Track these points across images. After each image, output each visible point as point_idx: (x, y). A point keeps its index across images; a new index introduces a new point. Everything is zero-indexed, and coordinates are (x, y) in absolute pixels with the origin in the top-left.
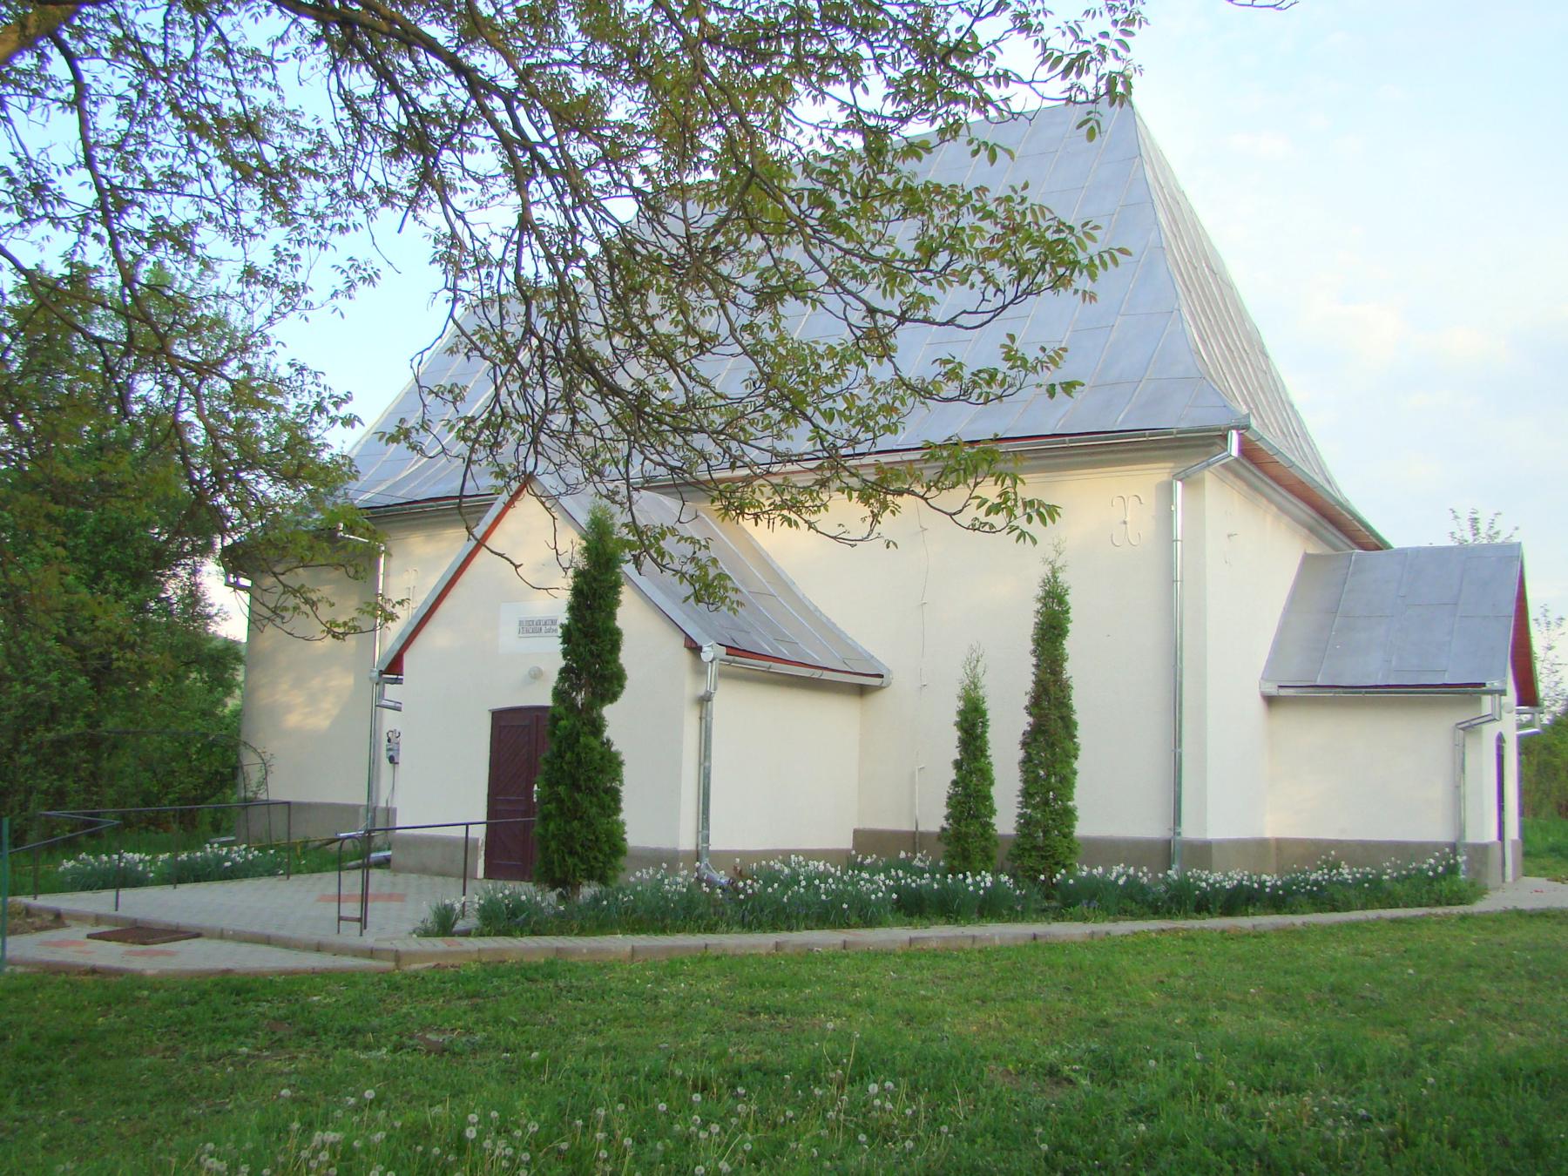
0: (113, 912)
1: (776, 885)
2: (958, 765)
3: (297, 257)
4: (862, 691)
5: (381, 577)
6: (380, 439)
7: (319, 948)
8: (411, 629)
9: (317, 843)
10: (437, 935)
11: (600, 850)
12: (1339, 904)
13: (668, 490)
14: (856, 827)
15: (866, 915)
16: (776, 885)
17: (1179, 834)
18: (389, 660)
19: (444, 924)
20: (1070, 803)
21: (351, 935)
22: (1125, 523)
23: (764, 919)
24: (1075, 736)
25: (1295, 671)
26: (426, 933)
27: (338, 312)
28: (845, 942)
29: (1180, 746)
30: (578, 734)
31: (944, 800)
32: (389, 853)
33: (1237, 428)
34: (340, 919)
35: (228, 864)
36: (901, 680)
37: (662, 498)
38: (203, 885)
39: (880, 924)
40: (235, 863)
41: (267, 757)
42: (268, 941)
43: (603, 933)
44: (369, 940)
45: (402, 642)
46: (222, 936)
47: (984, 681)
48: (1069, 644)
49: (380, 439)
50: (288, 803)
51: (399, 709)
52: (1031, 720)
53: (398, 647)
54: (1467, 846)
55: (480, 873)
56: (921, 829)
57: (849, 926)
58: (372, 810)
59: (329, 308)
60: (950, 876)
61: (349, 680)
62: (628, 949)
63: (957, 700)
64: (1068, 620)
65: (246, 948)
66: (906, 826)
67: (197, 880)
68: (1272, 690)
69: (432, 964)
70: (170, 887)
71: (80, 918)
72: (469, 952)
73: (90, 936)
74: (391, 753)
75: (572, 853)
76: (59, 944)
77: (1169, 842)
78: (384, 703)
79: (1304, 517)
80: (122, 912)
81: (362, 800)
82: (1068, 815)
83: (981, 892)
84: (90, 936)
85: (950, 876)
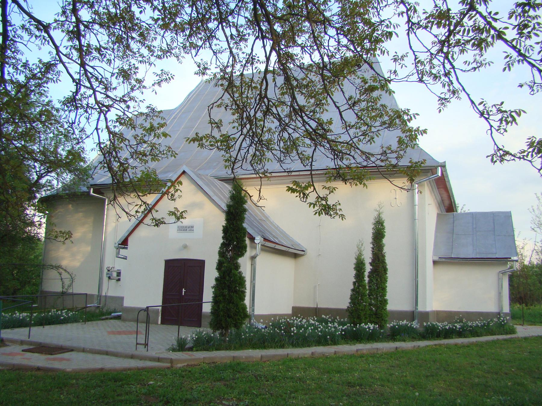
0: (27, 339)
1: (303, 329)
2: (354, 283)
3: (137, 68)
4: (295, 256)
5: (106, 210)
6: (187, 141)
7: (132, 357)
8: (132, 228)
9: (80, 308)
10: (179, 351)
11: (240, 316)
12: (479, 334)
13: (229, 181)
14: (293, 306)
15: (334, 341)
16: (303, 329)
17: (417, 309)
18: (122, 240)
19: (181, 346)
20: (385, 298)
21: (141, 351)
22: (396, 198)
23: (300, 343)
24: (387, 274)
25: (444, 252)
26: (174, 350)
27: (154, 91)
28: (335, 351)
29: (417, 278)
30: (231, 270)
31: (349, 297)
32: (120, 313)
33: (441, 166)
34: (137, 344)
35: (62, 318)
36: (311, 253)
37: (225, 184)
38: (53, 326)
39: (339, 344)
40: (65, 317)
41: (73, 276)
42: (107, 353)
43: (242, 349)
44: (152, 353)
45: (128, 233)
46: (84, 350)
47: (364, 253)
48: (384, 241)
49: (187, 141)
50: (86, 294)
51: (126, 259)
52: (371, 267)
53: (127, 235)
54: (503, 313)
55: (159, 322)
56: (318, 307)
57: (328, 345)
58: (99, 296)
59: (151, 90)
60: (358, 325)
61: (89, 249)
62: (260, 356)
63: (355, 259)
64: (385, 232)
65: (98, 357)
66: (312, 305)
67: (49, 324)
68: (436, 258)
69: (186, 364)
70: (41, 327)
71: (14, 342)
72: (200, 359)
73: (23, 351)
74: (108, 275)
75: (229, 317)
76: (10, 354)
77: (413, 312)
78: (120, 256)
79: (439, 201)
80: (32, 339)
81: (96, 292)
82: (385, 302)
83: (371, 331)
84: (23, 351)
85: (358, 325)
